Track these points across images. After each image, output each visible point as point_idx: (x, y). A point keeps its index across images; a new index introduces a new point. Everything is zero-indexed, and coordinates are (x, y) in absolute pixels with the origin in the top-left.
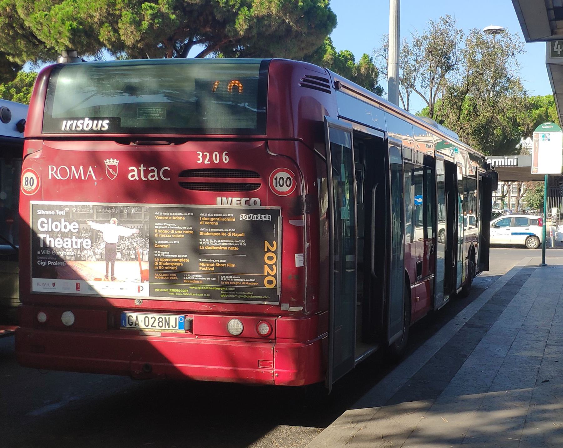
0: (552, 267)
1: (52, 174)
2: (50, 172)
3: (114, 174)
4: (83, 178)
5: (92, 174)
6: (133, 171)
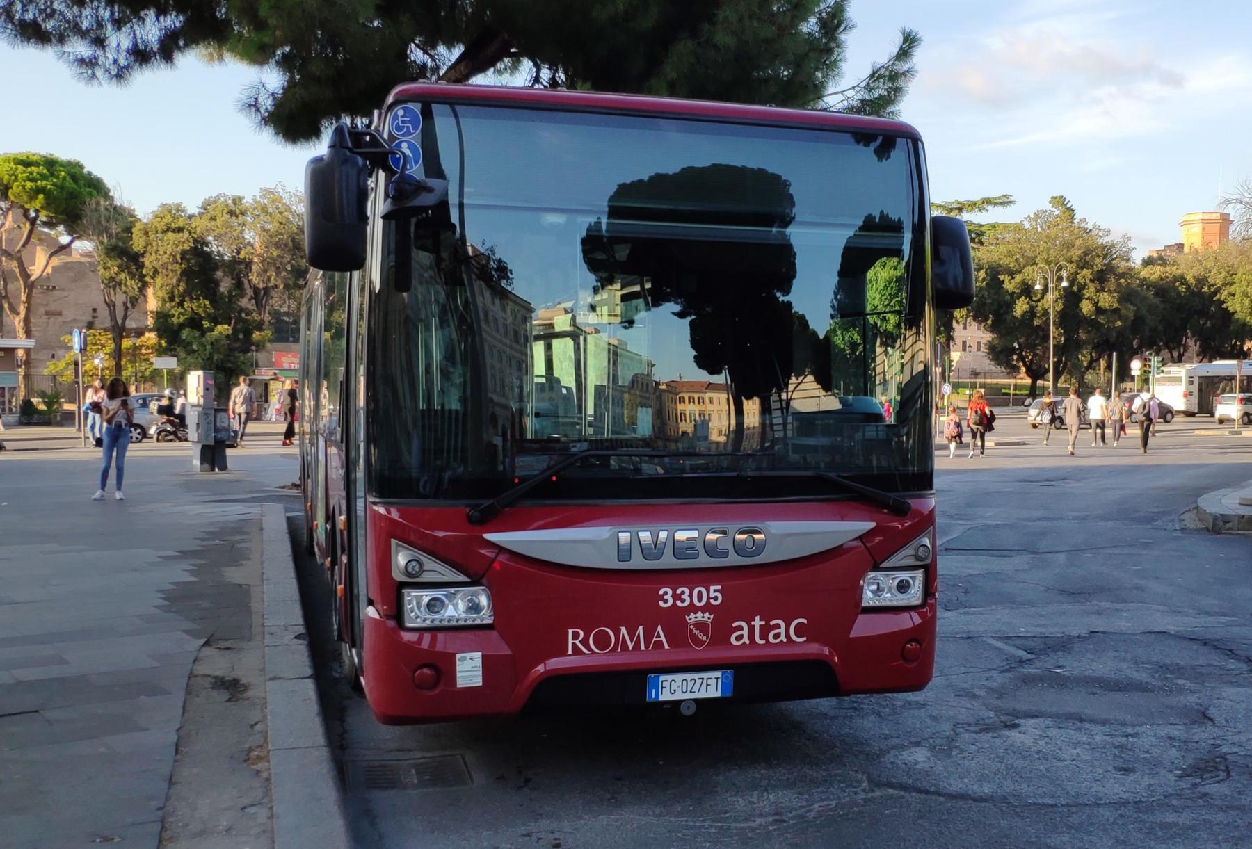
1: (574, 644)
4: (643, 648)
5: (663, 638)
6: (741, 628)
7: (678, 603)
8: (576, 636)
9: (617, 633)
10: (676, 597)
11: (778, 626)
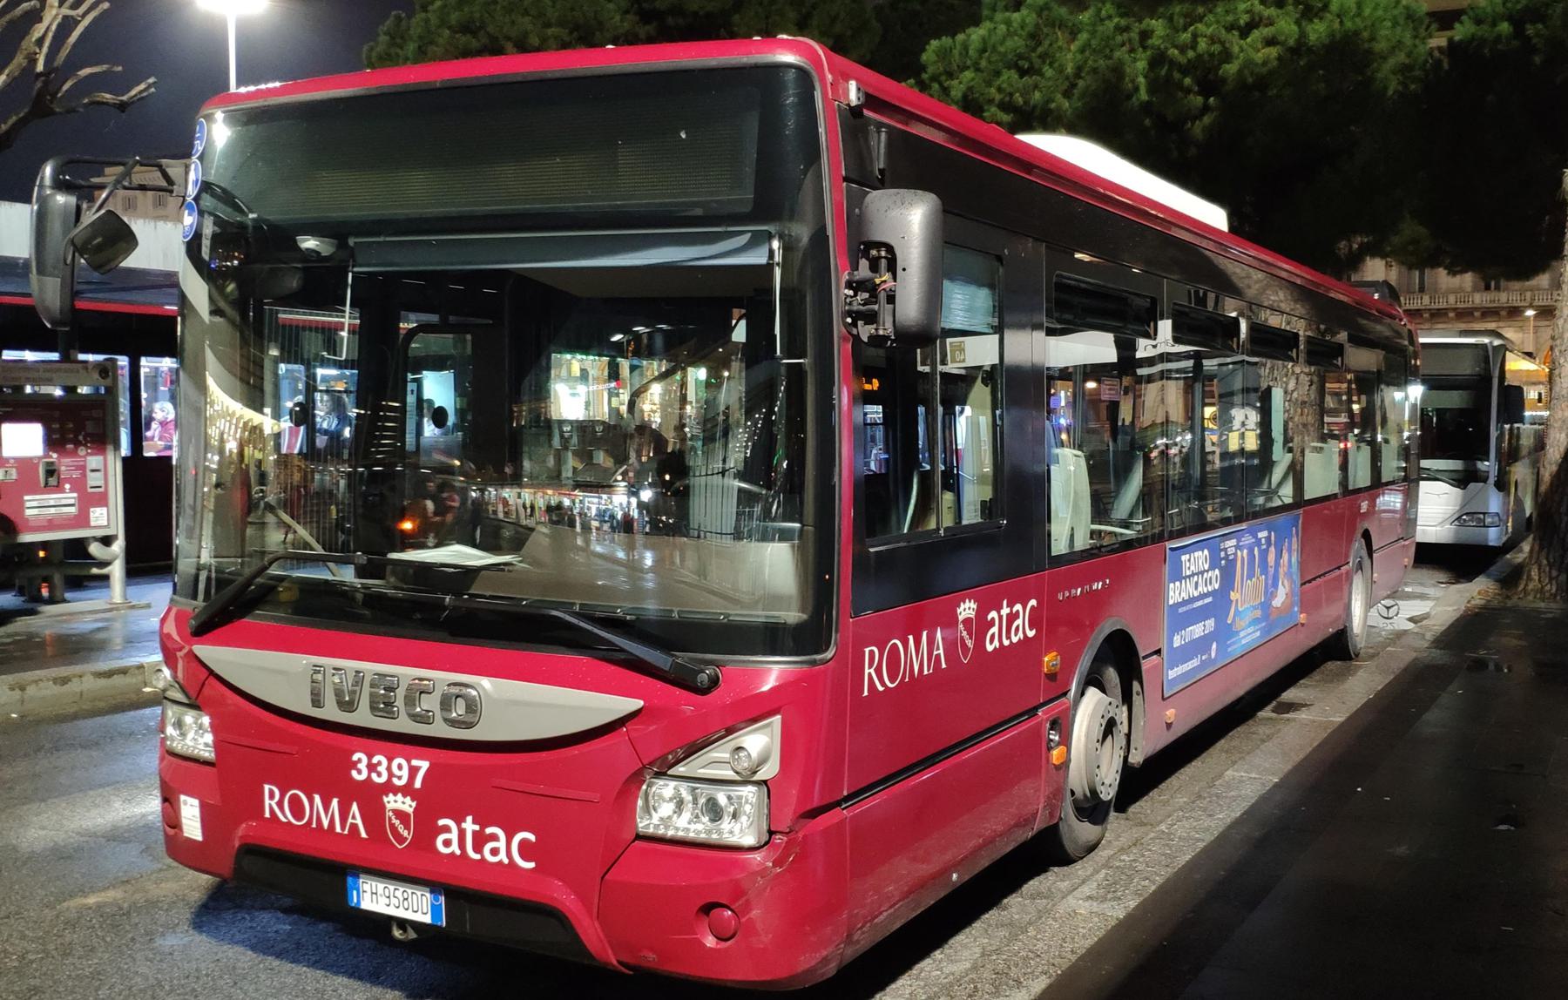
0: (980, 284)
2: (867, 671)
3: (405, 834)
4: (338, 829)
5: (359, 821)
6: (447, 829)
7: (374, 776)
10: (372, 768)
11: (494, 838)
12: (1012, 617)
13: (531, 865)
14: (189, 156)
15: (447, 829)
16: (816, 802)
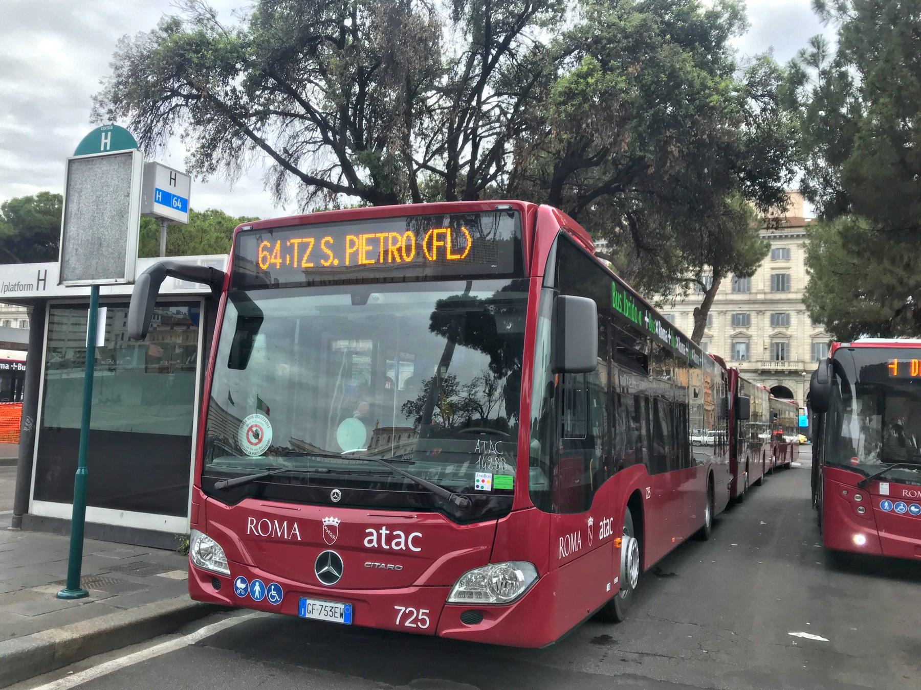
5: (297, 532)
6: (371, 534)
8: (252, 523)
9: (273, 524)
11: (399, 536)
12: (606, 524)
13: (419, 549)
14: (584, 448)
15: (371, 534)
16: (212, 404)
